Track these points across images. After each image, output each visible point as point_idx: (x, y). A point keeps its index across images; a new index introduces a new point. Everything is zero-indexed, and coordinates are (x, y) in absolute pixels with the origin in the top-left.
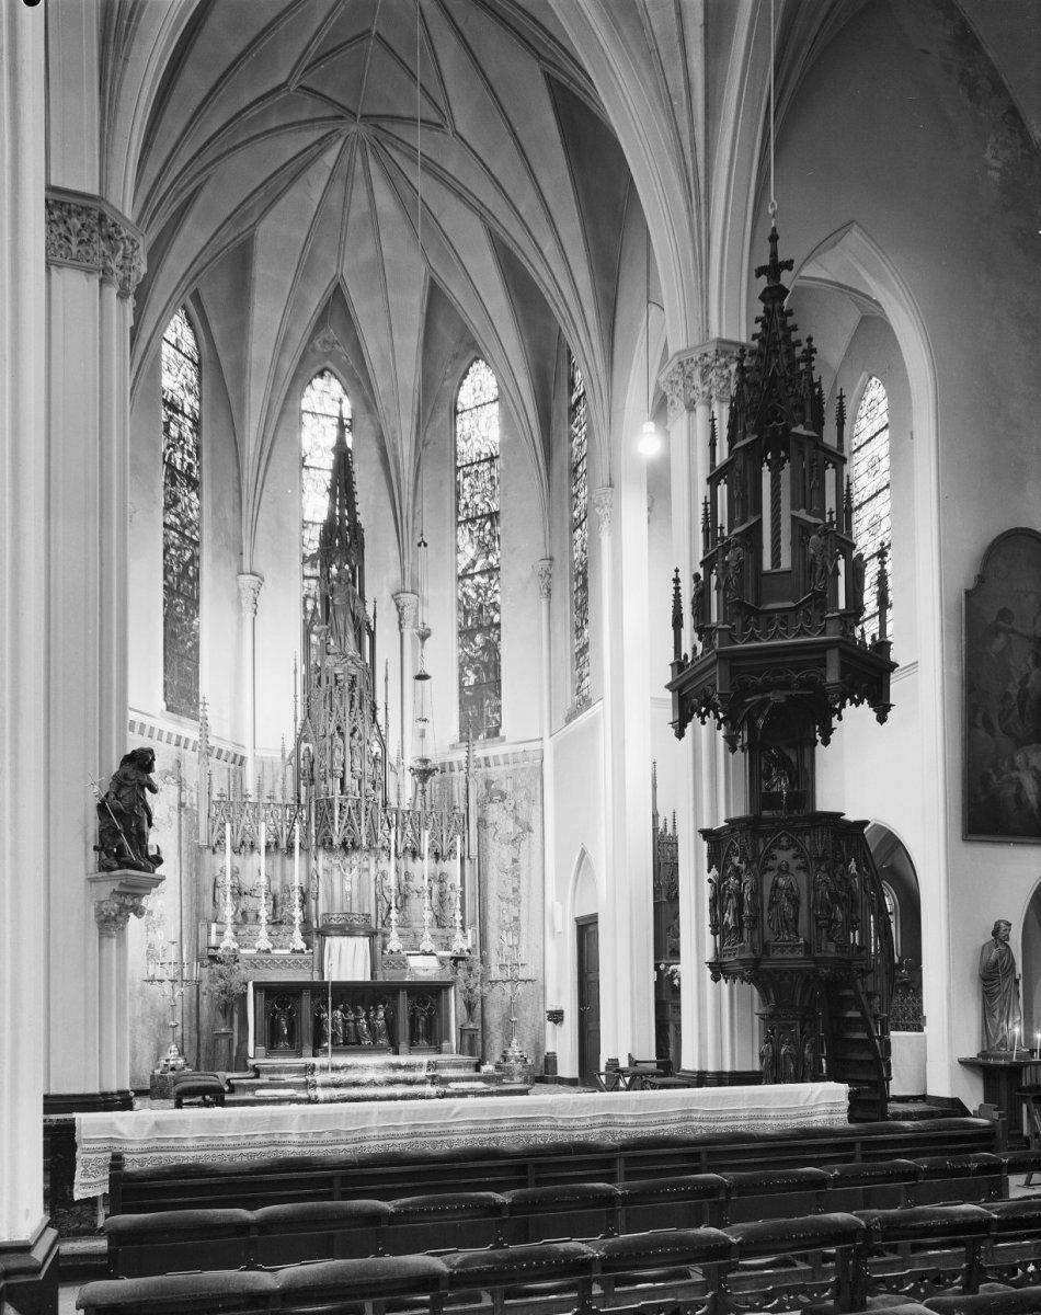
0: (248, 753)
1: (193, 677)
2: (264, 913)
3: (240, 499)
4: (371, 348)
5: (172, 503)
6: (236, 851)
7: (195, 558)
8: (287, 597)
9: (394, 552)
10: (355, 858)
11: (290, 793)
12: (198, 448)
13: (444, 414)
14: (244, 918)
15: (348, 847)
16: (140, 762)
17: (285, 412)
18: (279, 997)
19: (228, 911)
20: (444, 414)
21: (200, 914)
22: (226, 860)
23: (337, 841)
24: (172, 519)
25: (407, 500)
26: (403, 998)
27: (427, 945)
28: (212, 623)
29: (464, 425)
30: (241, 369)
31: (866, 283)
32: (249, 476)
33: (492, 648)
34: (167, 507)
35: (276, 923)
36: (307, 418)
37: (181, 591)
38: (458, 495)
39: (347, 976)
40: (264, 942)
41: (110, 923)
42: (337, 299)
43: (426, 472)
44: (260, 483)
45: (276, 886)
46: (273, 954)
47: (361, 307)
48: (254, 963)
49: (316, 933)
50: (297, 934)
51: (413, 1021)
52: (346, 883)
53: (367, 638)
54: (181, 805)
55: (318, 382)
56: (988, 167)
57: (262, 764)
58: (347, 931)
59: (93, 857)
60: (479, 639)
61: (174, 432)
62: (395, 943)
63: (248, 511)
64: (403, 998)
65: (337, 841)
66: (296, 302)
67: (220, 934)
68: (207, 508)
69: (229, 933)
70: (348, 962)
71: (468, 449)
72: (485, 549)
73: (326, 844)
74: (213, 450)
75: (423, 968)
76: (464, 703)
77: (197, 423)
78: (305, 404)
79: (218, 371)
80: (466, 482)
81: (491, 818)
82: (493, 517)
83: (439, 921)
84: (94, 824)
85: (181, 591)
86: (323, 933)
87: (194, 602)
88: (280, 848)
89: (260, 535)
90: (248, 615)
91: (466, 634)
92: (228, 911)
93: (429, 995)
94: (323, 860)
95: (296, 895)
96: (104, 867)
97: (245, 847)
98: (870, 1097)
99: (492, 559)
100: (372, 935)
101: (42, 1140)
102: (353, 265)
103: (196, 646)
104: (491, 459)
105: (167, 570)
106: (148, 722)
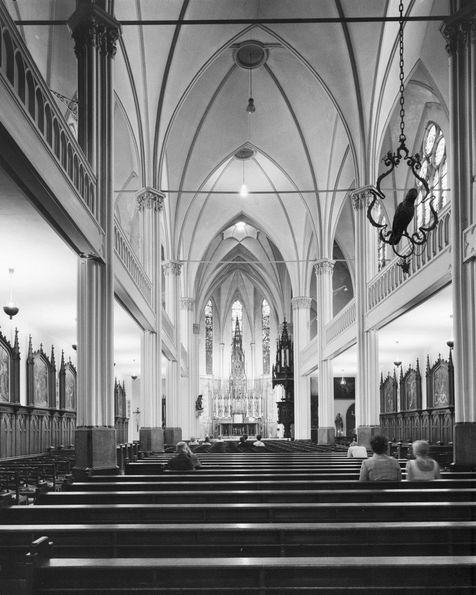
0: (222, 378)
1: (211, 366)
2: (223, 411)
3: (221, 330)
4: (244, 298)
5: (207, 335)
6: (219, 399)
7: (212, 344)
8: (229, 349)
9: (250, 335)
10: (240, 400)
11: (228, 387)
12: (212, 323)
13: (260, 307)
14: (220, 411)
15: (238, 398)
16: (201, 396)
17: (229, 309)
18: (226, 426)
19: (217, 410)
20: (260, 307)
21: (213, 411)
22: (217, 400)
23: (236, 397)
24: (208, 338)
25: (253, 325)
26: (247, 426)
27: (254, 416)
28: (215, 356)
29: (264, 309)
30: (219, 307)
31: (195, 445)
32: (221, 325)
33: (269, 355)
34: (206, 337)
35: (226, 412)
36: (233, 310)
37: (209, 350)
38: (263, 323)
39: (238, 422)
40: (223, 416)
41: (197, 417)
42: (237, 290)
43: (256, 319)
44: (224, 325)
45: (226, 405)
46: (226, 418)
47: (242, 292)
48: (221, 420)
49: (233, 414)
50: (229, 414)
51: (250, 431)
52: (238, 405)
53: (243, 356)
54: (209, 391)
55: (235, 302)
56: (340, 280)
57: (224, 381)
58: (238, 413)
59: (195, 409)
60: (266, 353)
61: (207, 322)
62: (247, 416)
63: (221, 332)
64: (247, 426)
65: (236, 397)
66: (229, 294)
67: (216, 414)
68: (214, 334)
69: (217, 414)
70: (238, 419)
71: (265, 314)
72: (268, 335)
73: (234, 397)
74: (215, 323)
75: (251, 420)
76: (264, 365)
77: (212, 318)
78: (233, 308)
79: (216, 308)
80: (264, 321)
81: (268, 390)
82: (269, 328)
83: (257, 411)
84: (195, 405)
85: (209, 350)
86: (234, 414)
87: (211, 352)
88: (226, 398)
89: (224, 336)
90: (221, 352)
91: (264, 352)
92: (217, 410)
93: (252, 426)
94: (234, 400)
95: (229, 407)
96: (196, 410)
97: (220, 398)
98: (293, 439)
99: (269, 337)
100: (243, 414)
101: (262, 368)
102: (239, 286)
103: (212, 360)
104: (268, 317)
105: (206, 348)
106: (203, 377)
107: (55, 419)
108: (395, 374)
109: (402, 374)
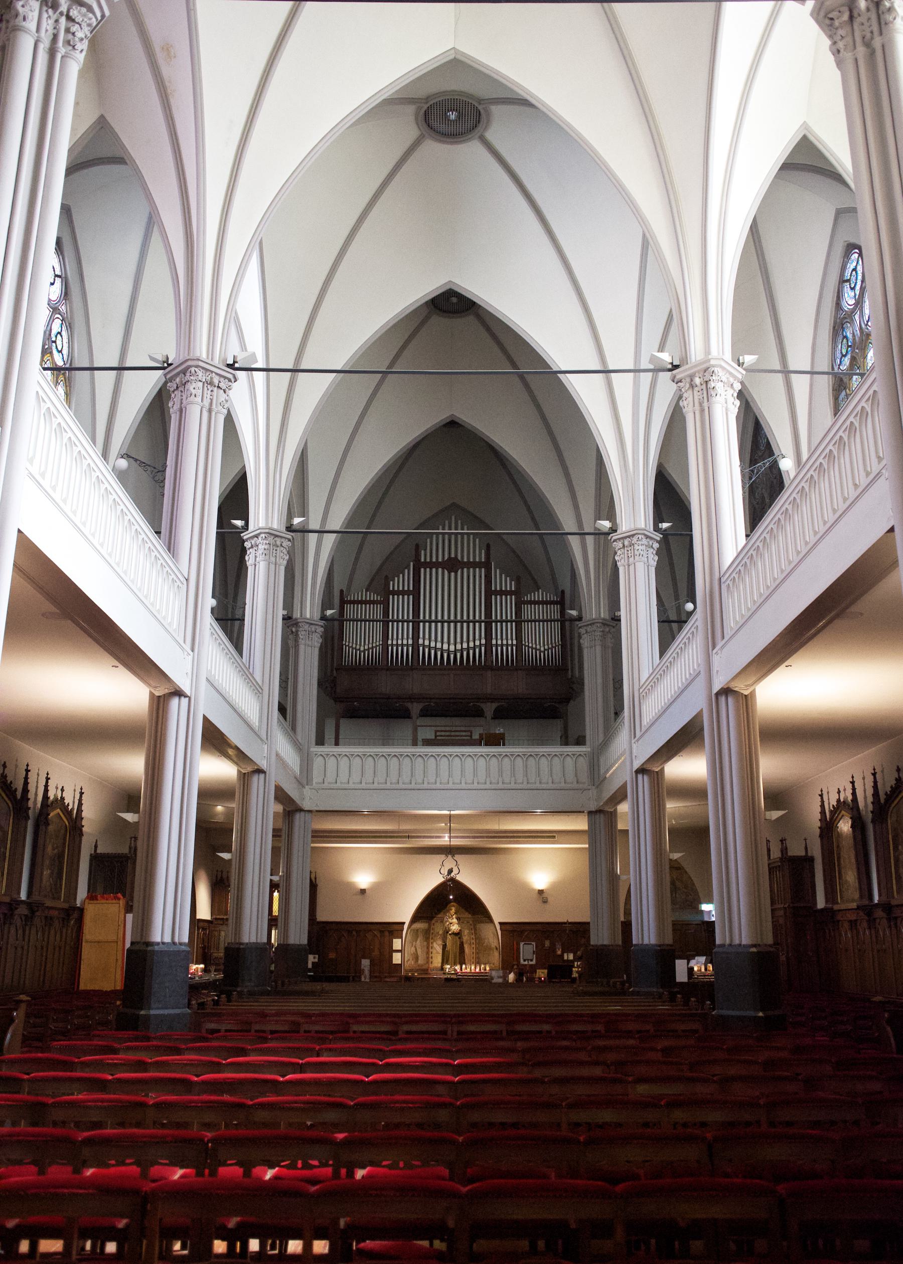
107: (17, 921)
108: (854, 793)
109: (823, 812)
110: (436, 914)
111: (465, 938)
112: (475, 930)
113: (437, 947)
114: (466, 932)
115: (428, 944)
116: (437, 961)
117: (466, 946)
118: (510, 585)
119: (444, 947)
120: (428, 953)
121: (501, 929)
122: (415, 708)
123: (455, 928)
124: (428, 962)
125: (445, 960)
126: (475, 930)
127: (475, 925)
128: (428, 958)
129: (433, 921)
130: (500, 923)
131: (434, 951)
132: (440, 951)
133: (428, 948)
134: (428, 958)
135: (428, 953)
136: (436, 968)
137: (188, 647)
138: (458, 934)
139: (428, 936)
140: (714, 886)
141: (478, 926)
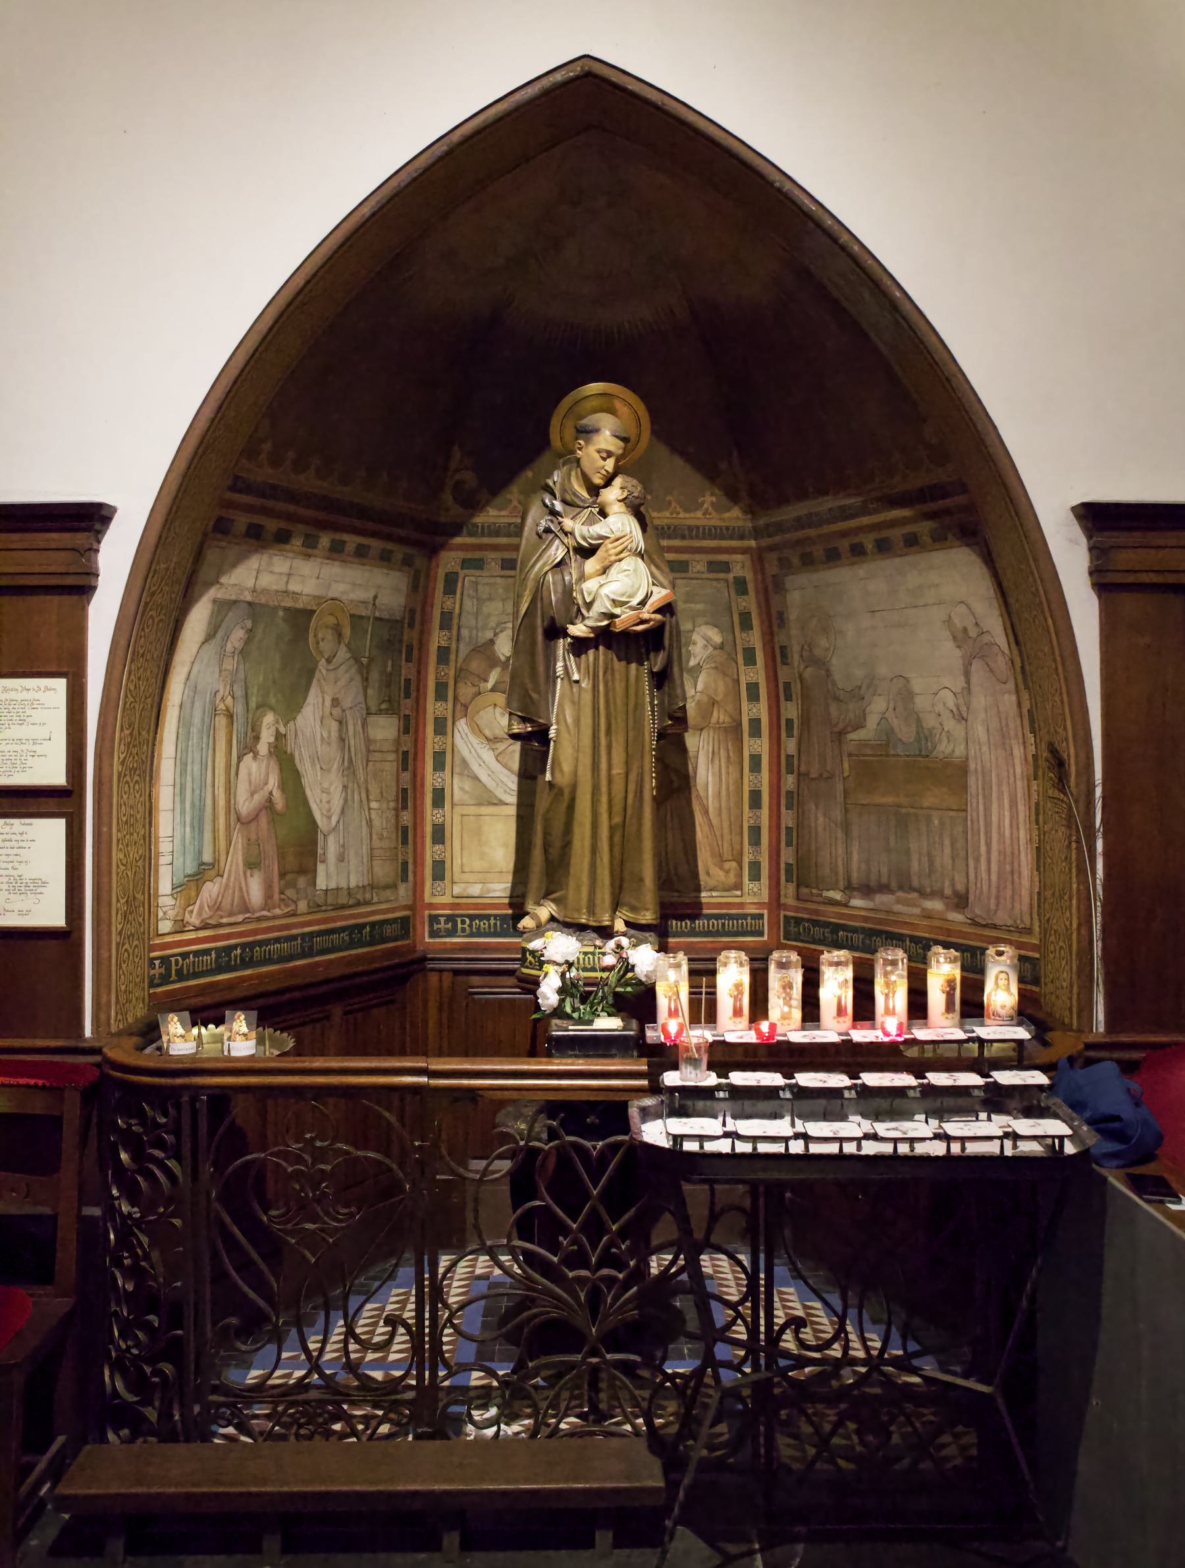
110: (473, 504)
111: (697, 689)
112: (774, 621)
113: (481, 757)
114: (701, 643)
115: (411, 726)
116: (481, 858)
117: (702, 749)
118: (295, 1427)
119: (535, 742)
120: (407, 798)
121: (1105, 584)
122: (406, 776)
123: (623, 586)
124: (408, 870)
125: (542, 859)
126: (774, 621)
127: (771, 591)
128: (407, 835)
129: (449, 560)
130: (1097, 518)
131: (459, 789)
132: (506, 785)
133: (409, 760)
134: (407, 835)
135: (407, 798)
136: (472, 916)
137: (299, 733)
138: (642, 645)
139: (402, 667)
140: (607, 872)
141: (800, 590)
